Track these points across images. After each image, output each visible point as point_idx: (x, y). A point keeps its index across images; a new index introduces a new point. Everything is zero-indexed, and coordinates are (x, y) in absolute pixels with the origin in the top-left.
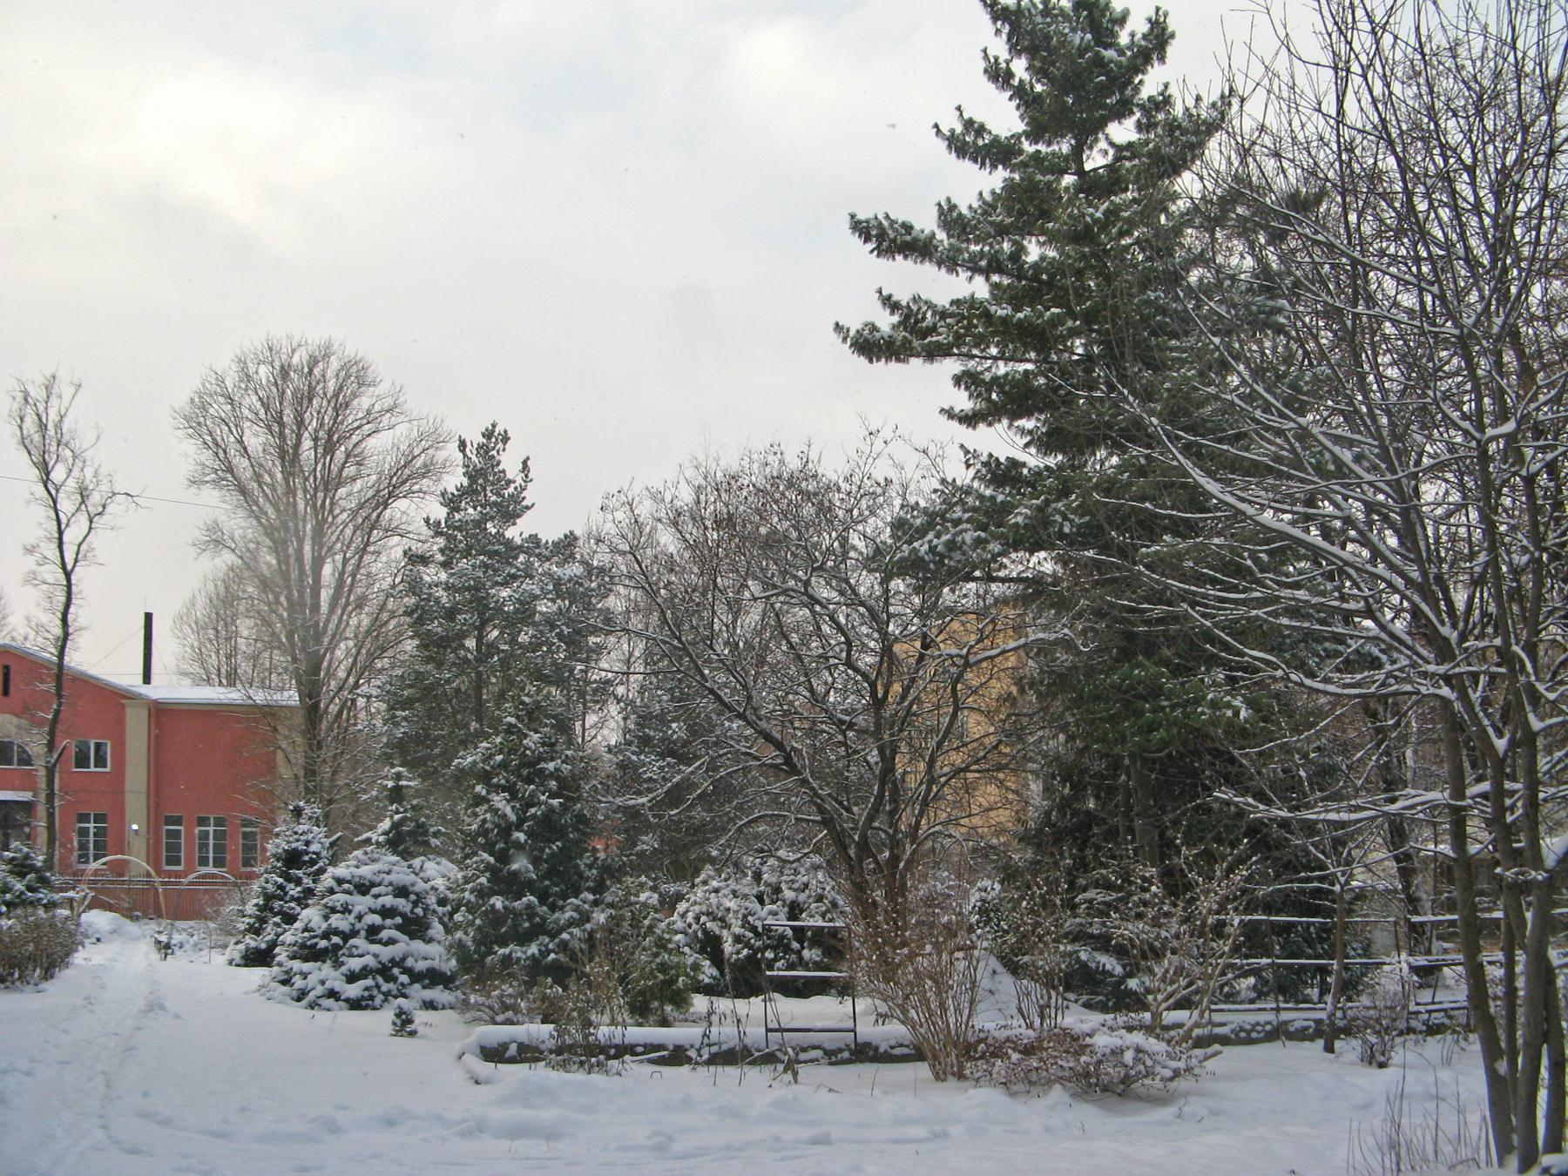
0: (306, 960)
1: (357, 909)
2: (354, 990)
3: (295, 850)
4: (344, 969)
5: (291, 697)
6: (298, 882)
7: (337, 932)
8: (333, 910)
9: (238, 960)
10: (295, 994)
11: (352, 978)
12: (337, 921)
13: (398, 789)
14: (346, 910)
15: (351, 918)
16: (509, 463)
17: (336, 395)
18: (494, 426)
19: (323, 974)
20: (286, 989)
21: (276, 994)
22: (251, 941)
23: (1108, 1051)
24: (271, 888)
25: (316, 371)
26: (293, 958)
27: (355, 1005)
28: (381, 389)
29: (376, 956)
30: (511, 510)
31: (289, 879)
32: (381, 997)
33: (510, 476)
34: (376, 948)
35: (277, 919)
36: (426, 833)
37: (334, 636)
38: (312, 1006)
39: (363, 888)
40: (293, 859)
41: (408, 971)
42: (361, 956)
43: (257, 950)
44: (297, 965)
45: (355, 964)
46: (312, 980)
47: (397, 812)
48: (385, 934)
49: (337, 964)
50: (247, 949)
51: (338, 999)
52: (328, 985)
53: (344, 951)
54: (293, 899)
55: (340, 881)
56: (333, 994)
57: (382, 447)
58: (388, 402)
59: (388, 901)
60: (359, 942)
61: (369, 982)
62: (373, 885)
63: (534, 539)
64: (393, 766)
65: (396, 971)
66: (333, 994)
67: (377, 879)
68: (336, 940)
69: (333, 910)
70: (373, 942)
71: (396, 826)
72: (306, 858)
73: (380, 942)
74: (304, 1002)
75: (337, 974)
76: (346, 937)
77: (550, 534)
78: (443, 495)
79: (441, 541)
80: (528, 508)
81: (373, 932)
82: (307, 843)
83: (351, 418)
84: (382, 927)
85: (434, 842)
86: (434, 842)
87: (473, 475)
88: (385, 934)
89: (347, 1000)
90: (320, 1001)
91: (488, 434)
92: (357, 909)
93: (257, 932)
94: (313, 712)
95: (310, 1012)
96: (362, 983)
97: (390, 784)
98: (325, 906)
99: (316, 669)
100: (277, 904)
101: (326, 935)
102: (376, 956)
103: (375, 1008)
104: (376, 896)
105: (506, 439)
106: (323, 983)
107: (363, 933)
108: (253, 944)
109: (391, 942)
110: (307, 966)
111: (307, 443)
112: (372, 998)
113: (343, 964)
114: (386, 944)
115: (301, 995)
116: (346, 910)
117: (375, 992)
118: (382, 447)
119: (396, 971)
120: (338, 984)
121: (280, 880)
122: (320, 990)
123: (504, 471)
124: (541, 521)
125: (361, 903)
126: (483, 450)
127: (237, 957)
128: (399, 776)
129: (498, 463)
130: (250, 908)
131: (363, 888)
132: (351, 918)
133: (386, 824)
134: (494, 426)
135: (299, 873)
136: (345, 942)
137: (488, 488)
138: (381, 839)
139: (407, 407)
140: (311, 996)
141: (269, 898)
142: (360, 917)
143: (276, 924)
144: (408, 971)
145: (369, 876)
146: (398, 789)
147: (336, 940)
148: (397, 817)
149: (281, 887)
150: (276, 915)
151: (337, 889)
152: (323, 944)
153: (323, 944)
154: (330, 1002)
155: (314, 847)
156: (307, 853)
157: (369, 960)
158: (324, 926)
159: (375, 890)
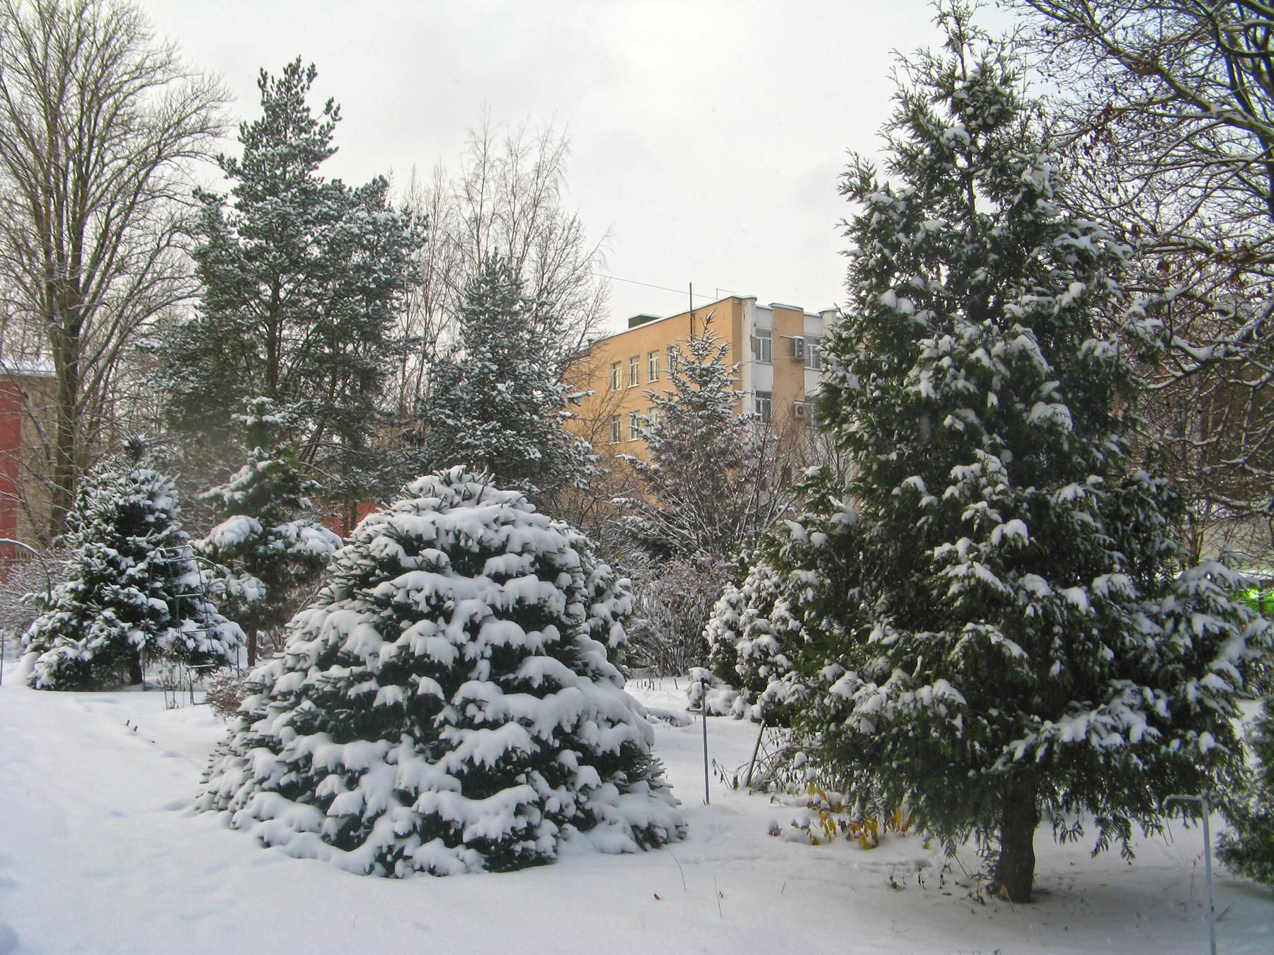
0: (341, 736)
1: (466, 608)
2: (490, 816)
3: (135, 506)
4: (452, 759)
5: (46, 365)
6: (139, 554)
7: (426, 666)
8: (408, 613)
9: (45, 679)
10: (330, 826)
11: (478, 782)
12: (417, 636)
13: (261, 427)
14: (439, 610)
15: (456, 630)
16: (314, 100)
17: (106, 44)
18: (299, 61)
19: (390, 772)
20: (302, 812)
21: (278, 827)
22: (64, 649)
23: (593, 666)
24: (97, 565)
25: (86, 15)
26: (304, 727)
27: (502, 856)
28: (154, 44)
29: (527, 723)
30: (314, 154)
31: (125, 552)
32: (549, 827)
33: (312, 116)
34: (521, 703)
35: (109, 613)
36: (295, 490)
37: (95, 295)
38: (387, 863)
39: (467, 559)
40: (130, 520)
41: (588, 756)
42: (494, 725)
43: (78, 663)
44: (322, 749)
45: (484, 746)
46: (375, 788)
47: (261, 459)
48: (536, 667)
49: (434, 749)
50: (61, 662)
51: (453, 840)
52: (425, 803)
53: (447, 713)
54: (132, 581)
55: (412, 544)
56: (435, 827)
57: (150, 102)
58: (162, 57)
59: (530, 587)
60: (478, 687)
61: (522, 792)
62: (487, 552)
63: (338, 186)
64: (254, 395)
65: (569, 758)
66: (435, 827)
67: (496, 539)
68: (427, 685)
69: (408, 613)
70: (508, 688)
71: (258, 477)
72: (151, 519)
73: (525, 687)
74: (364, 854)
75: (435, 772)
76: (454, 674)
77: (355, 181)
78: (242, 129)
79: (236, 182)
80: (331, 152)
81: (505, 662)
82: (152, 496)
83: (119, 71)
84: (524, 653)
85: (305, 501)
86: (305, 501)
87: (273, 109)
88: (536, 667)
89: (480, 844)
90: (410, 847)
91: (293, 70)
92: (466, 608)
93: (77, 633)
94: (69, 379)
95: (377, 884)
96: (508, 796)
97: (250, 420)
98: (384, 602)
99: (74, 329)
100: (108, 591)
101: (394, 673)
102: (527, 723)
103: (541, 860)
104: (500, 578)
105: (312, 75)
106: (407, 798)
107: (484, 666)
108: (71, 653)
109: (550, 686)
110: (354, 753)
111: (73, 89)
112: (530, 832)
113: (449, 746)
114: (540, 693)
115: (349, 834)
116: (439, 610)
117: (536, 816)
118: (150, 102)
119: (569, 758)
120: (451, 804)
121: (113, 552)
122: (400, 818)
123: (308, 110)
124: (344, 168)
125: (472, 595)
126: (287, 86)
127: (43, 673)
128: (261, 409)
129: (302, 102)
130: (62, 592)
131: (467, 559)
132: (456, 630)
133: (245, 474)
134: (299, 61)
135: (142, 541)
136: (450, 691)
137: (287, 126)
138: (238, 495)
139: (182, 63)
140: (382, 833)
141: (93, 580)
142: (473, 628)
143: (109, 622)
144: (588, 756)
145: (480, 531)
146: (261, 427)
147: (427, 685)
148: (262, 465)
149: (113, 563)
150: (105, 605)
151: (407, 561)
152: (390, 694)
153: (390, 694)
154: (433, 851)
155: (162, 503)
156: (152, 511)
157: (513, 736)
158: (388, 651)
159: (495, 564)
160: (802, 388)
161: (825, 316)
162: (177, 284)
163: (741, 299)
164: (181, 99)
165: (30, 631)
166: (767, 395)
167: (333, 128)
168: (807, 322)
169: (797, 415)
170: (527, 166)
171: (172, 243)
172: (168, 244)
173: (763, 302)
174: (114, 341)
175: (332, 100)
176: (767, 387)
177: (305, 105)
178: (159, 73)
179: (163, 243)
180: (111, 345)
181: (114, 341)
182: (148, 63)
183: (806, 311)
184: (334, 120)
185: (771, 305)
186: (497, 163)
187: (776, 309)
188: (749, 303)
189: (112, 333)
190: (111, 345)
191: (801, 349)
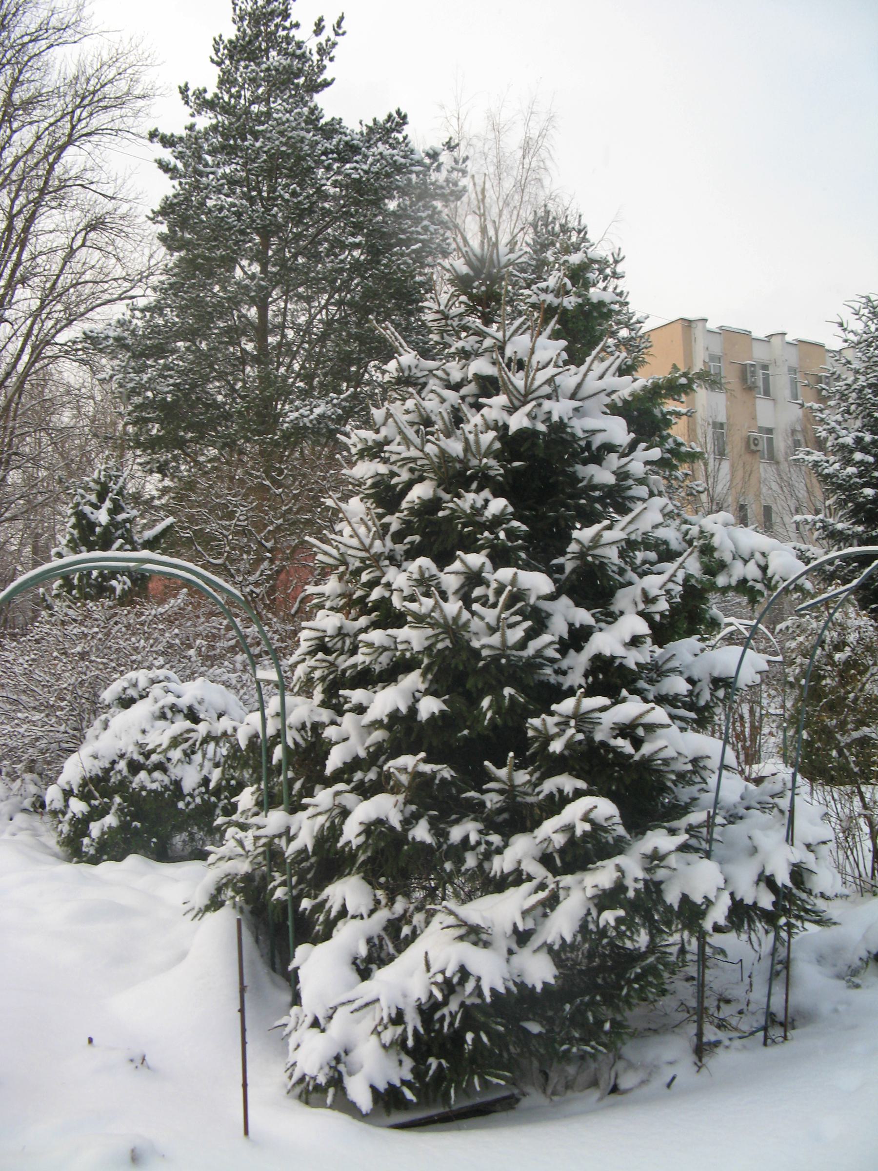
9: (374, 1067)
57: (61, 64)
123: (297, 25)
124: (348, 101)
160: (754, 418)
161: (773, 340)
162: (99, 288)
163: (690, 321)
164: (96, 65)
165: (62, 780)
166: (721, 425)
167: (334, 44)
168: (755, 345)
169: (753, 447)
170: (512, 143)
171: (88, 243)
172: (83, 245)
173: (711, 325)
174: (25, 358)
175: (321, 20)
176: (722, 418)
177: (293, 19)
178: (70, 31)
179: (78, 242)
180: (20, 367)
181: (25, 358)
182: (54, 22)
183: (755, 335)
184: (337, 34)
185: (720, 328)
186: (474, 141)
187: (726, 333)
188: (700, 324)
189: (22, 350)
190: (20, 367)
191: (753, 374)
